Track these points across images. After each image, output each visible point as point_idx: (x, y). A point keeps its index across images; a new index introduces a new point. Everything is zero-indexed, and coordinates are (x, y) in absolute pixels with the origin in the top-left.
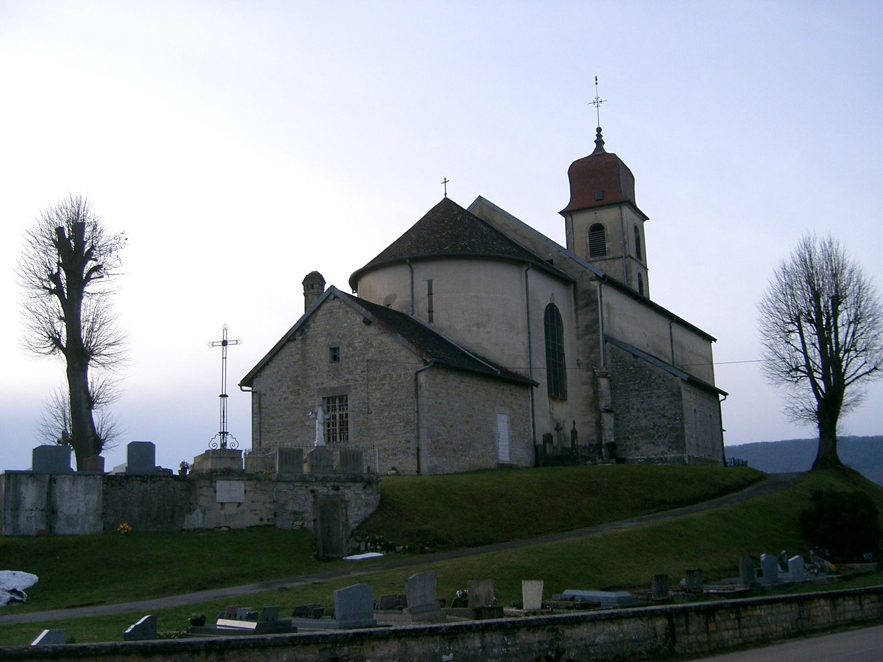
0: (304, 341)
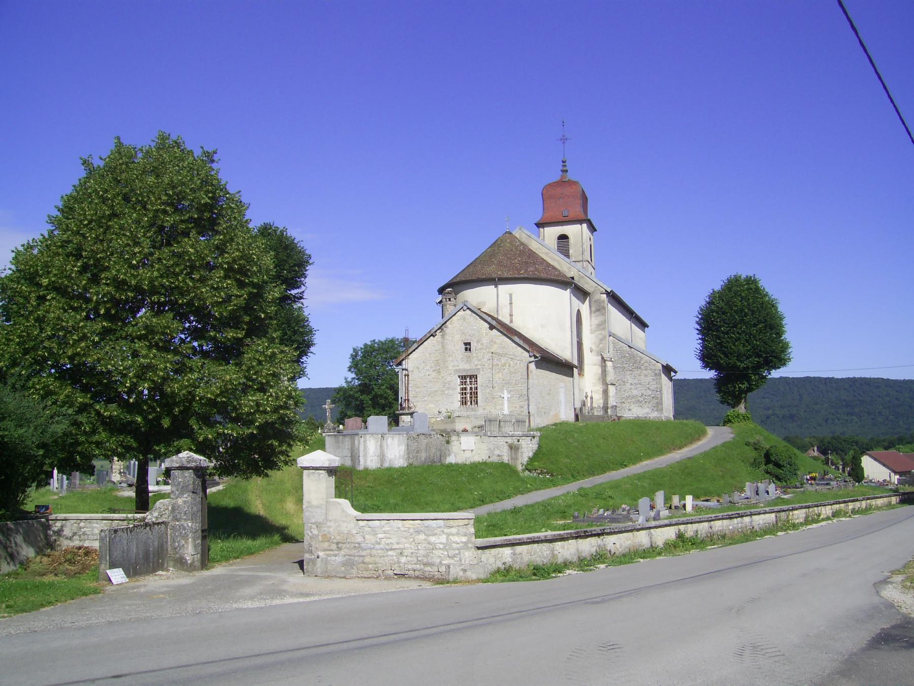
0: (443, 336)
